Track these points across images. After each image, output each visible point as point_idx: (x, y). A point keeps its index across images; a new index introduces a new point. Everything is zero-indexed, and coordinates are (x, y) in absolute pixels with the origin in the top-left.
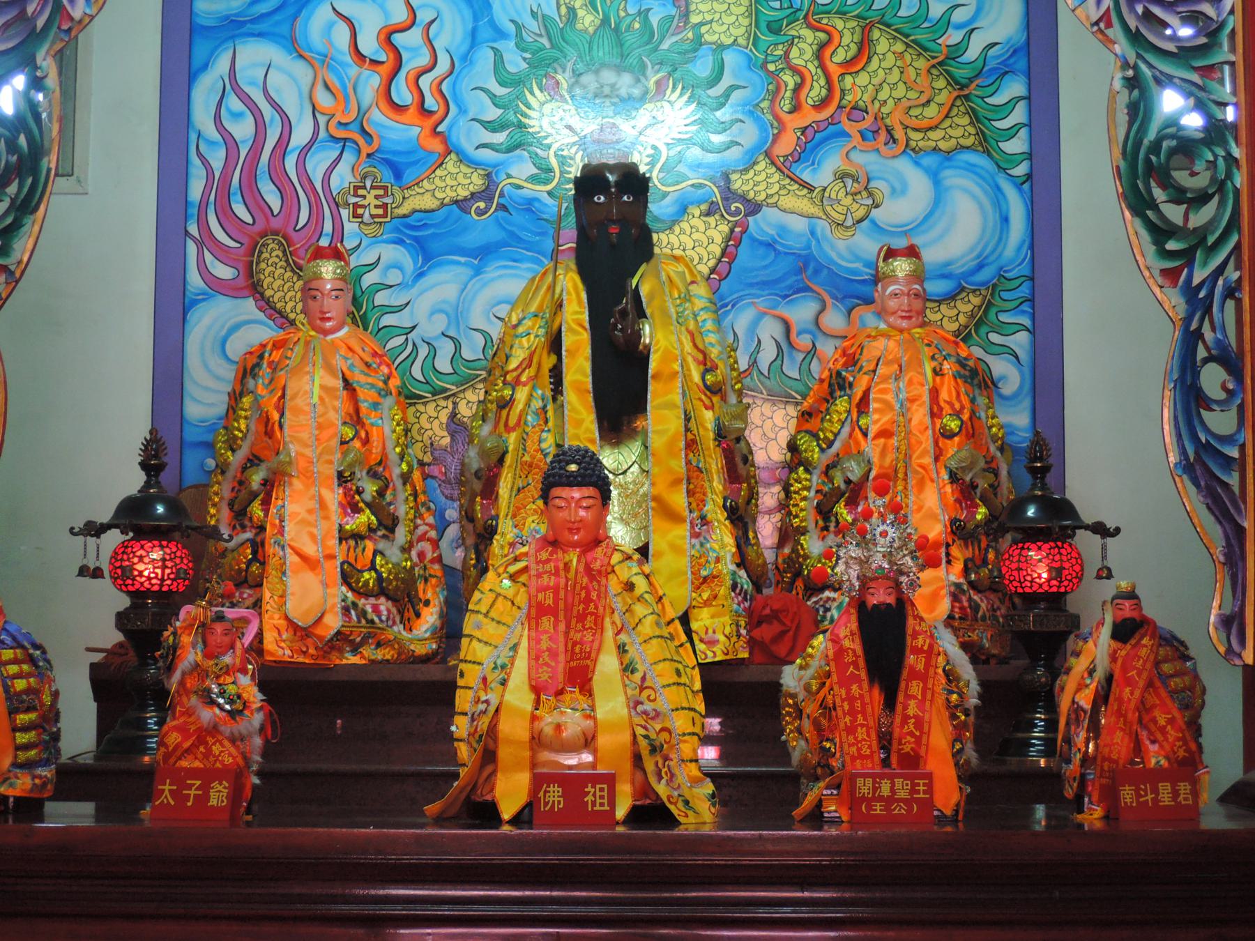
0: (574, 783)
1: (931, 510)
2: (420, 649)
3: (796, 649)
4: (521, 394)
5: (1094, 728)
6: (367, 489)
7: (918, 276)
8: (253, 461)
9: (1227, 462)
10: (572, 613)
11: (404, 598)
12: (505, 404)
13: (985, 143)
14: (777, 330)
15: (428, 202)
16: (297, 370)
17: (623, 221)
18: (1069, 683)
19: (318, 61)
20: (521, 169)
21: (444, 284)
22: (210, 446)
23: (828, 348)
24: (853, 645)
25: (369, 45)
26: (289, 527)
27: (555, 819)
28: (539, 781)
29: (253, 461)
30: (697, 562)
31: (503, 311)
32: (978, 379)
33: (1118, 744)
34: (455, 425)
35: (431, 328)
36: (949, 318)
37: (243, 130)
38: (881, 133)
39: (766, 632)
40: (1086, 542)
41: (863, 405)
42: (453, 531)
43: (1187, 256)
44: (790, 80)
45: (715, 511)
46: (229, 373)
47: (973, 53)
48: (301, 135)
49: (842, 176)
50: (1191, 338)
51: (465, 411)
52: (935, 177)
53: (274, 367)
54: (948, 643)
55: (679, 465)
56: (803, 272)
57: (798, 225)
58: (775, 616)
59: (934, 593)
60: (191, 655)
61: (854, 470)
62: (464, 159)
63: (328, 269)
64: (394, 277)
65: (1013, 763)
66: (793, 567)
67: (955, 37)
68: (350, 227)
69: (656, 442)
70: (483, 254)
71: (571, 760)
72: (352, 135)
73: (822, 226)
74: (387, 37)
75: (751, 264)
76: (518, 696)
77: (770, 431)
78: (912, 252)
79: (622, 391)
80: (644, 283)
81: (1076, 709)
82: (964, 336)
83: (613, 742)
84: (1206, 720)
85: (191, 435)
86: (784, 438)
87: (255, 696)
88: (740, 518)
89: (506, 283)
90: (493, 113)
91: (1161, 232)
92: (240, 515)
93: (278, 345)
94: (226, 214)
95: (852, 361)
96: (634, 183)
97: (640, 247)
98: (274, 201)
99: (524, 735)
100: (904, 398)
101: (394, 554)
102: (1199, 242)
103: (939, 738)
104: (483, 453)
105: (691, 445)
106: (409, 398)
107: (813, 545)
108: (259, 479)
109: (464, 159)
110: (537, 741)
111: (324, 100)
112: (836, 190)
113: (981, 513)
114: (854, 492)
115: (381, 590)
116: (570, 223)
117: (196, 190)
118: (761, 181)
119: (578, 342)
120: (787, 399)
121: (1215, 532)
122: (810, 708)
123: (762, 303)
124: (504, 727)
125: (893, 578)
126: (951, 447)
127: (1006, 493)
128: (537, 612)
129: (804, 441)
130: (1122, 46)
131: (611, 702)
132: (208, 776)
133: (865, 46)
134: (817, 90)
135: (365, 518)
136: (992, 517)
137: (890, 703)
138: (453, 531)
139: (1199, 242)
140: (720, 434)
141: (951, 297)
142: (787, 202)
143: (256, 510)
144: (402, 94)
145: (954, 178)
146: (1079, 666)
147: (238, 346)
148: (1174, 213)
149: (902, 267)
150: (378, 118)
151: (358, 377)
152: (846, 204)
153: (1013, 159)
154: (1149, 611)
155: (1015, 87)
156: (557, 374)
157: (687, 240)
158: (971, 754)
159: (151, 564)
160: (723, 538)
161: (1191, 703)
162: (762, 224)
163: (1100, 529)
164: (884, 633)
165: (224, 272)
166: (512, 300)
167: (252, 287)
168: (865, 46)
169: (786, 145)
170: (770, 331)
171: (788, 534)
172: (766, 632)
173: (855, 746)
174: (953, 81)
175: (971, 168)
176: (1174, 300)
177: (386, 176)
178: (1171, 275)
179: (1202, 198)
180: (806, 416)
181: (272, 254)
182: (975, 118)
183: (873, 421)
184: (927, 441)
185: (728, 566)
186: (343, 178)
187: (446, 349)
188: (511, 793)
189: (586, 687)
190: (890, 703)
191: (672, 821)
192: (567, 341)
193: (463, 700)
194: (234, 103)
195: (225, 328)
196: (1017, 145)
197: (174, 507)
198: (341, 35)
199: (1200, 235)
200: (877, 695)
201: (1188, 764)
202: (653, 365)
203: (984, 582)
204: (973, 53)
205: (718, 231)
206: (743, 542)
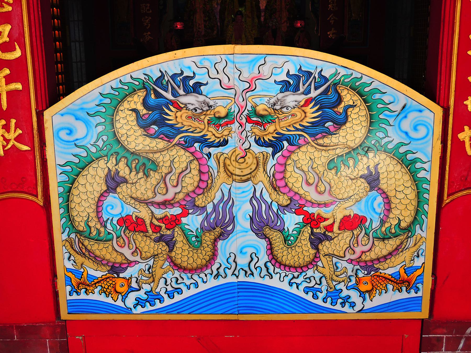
135: (207, 19)
160: (256, 20)
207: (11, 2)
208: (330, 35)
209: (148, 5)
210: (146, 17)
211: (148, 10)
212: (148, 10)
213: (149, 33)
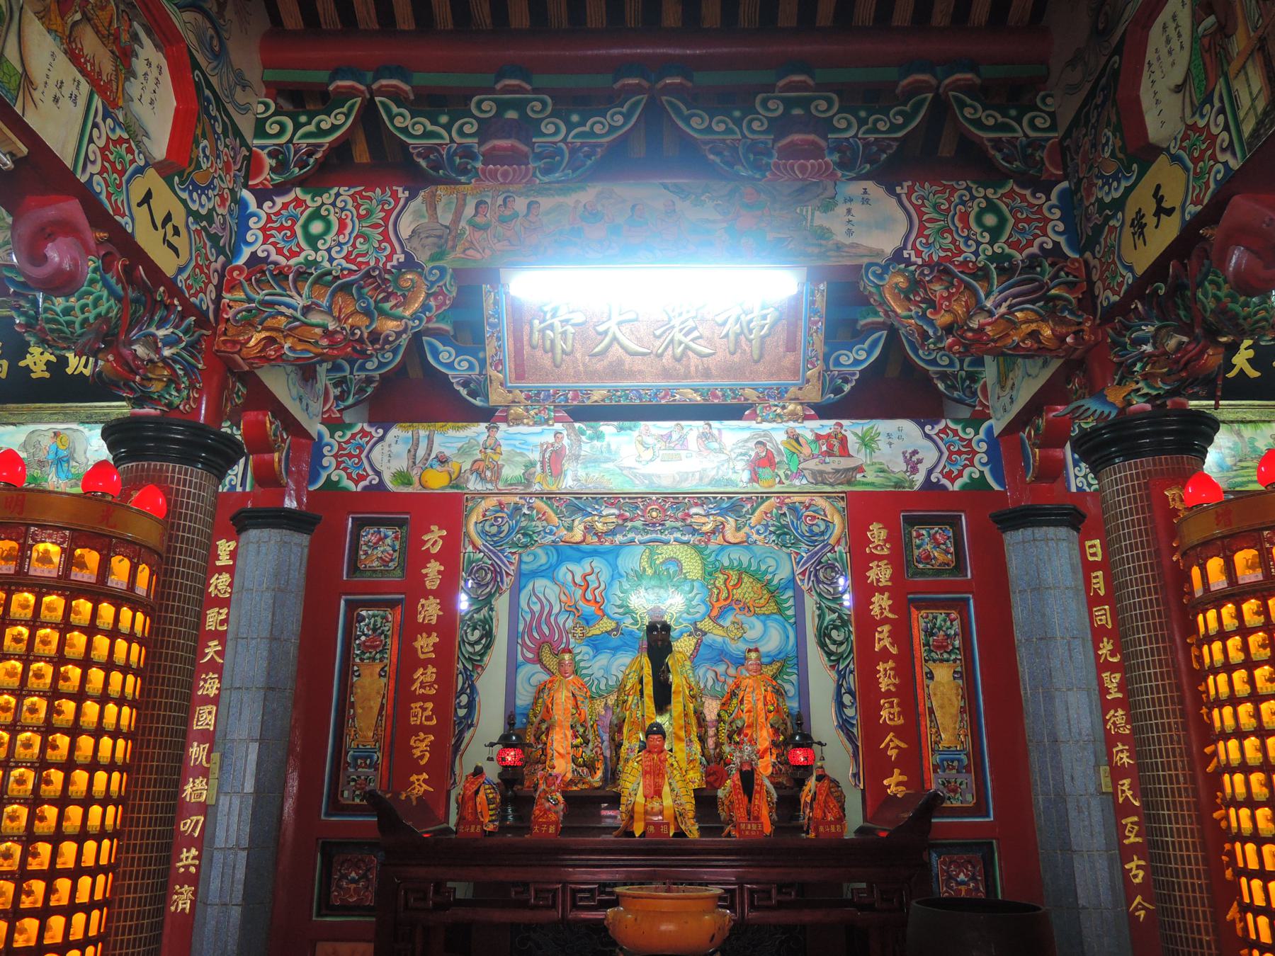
0: (657, 825)
1: (764, 737)
2: (596, 785)
3: (722, 784)
4: (630, 698)
5: (811, 808)
6: (580, 729)
7: (758, 658)
8: (543, 721)
9: (853, 725)
10: (655, 774)
11: (591, 767)
12: (625, 702)
13: (780, 611)
14: (713, 675)
15: (598, 632)
16: (557, 691)
17: (663, 640)
18: (804, 794)
19: (562, 585)
20: (628, 621)
21: (603, 659)
22: (527, 716)
23: (730, 681)
24: (739, 783)
25: (578, 580)
26: (555, 744)
27: (652, 835)
28: (647, 825)
29: (543, 721)
30: (689, 755)
31: (623, 668)
32: (779, 692)
33: (819, 813)
34: (606, 707)
35: (599, 674)
36: (769, 671)
37: (537, 608)
38: (746, 608)
39: (712, 779)
40: (815, 747)
41: (741, 702)
42: (606, 743)
43: (838, 661)
44: (716, 591)
45: (694, 737)
46: (534, 690)
47: (775, 582)
48: (556, 610)
49: (733, 623)
50: (840, 686)
51: (610, 702)
52: (764, 623)
53: (550, 689)
54: (767, 782)
55: (682, 722)
56: (721, 655)
57: (720, 639)
58: (714, 773)
59: (765, 767)
60: (543, 787)
61: (740, 724)
62: (609, 617)
63: (567, 657)
64: (586, 657)
65: (794, 823)
66: (720, 757)
67: (769, 577)
68: (572, 640)
69: (675, 714)
70: (615, 650)
71: (656, 819)
72: (573, 610)
73: (727, 639)
74: (584, 577)
75: (705, 653)
76: (640, 799)
77: (711, 709)
78: (756, 650)
79: (663, 698)
80: (670, 660)
81: (806, 802)
82: (775, 677)
83: (668, 813)
84: (846, 806)
85: (518, 711)
86: (716, 712)
87: (561, 799)
88: (702, 740)
89: (624, 659)
90: (619, 603)
91: (829, 654)
92: (538, 739)
93: (551, 682)
94: (531, 637)
95: (738, 687)
96: (666, 628)
97: (668, 649)
98: (547, 632)
99: (642, 811)
100: (755, 698)
101: (588, 752)
102: (841, 657)
103: (765, 812)
104: (618, 718)
105: (686, 715)
106: (592, 698)
107: (726, 749)
108: (545, 727)
109: (609, 617)
110: (646, 813)
111: (563, 598)
112: (732, 628)
113: (782, 738)
114: (740, 731)
115: (585, 765)
116: (645, 642)
117: (521, 628)
118: (706, 625)
119: (648, 679)
120: (716, 698)
121: (849, 746)
122: (726, 802)
123: (708, 665)
124: (637, 808)
125: (750, 762)
126: (771, 716)
127: (790, 731)
128: (645, 773)
129: (723, 713)
130: (816, 597)
131: (668, 801)
132: (549, 824)
133: (740, 580)
134: (724, 595)
135: (579, 740)
136: (785, 739)
137: (750, 801)
138: (606, 743)
139: (841, 657)
140: (695, 712)
141: (771, 663)
142: (715, 632)
143: (544, 737)
144: (589, 596)
145: (769, 623)
146: (806, 789)
147: (534, 681)
148: (833, 648)
149: (753, 655)
150: (581, 604)
151: (576, 692)
152: (735, 633)
153: (790, 617)
154: (827, 772)
155: (790, 593)
156: (642, 692)
157: (683, 645)
158: (775, 816)
159: (510, 757)
160: (697, 747)
161: (841, 800)
162: (708, 639)
163: (820, 743)
164: (748, 779)
165: (530, 655)
166: (627, 665)
167: (538, 660)
168: (740, 580)
169: (715, 613)
170: (710, 675)
171: (718, 745)
172: (712, 779)
173: (740, 814)
174: (769, 591)
175: (776, 620)
176: (834, 675)
177: (583, 622)
178: (833, 667)
179: (841, 643)
180: (723, 704)
181: (546, 649)
182: (777, 603)
183: (745, 707)
184: (763, 715)
185: (698, 756)
186: (569, 624)
187: (603, 681)
188: (638, 829)
189: (660, 797)
190: (750, 801)
191: (685, 836)
192: (645, 680)
193: (623, 800)
194: (534, 599)
195: (531, 676)
196: (791, 612)
197: (518, 737)
198: (569, 577)
199: (842, 654)
200: (746, 798)
201: (841, 819)
202: (673, 689)
203: (783, 761)
204: (775, 582)
205: (693, 641)
206: (703, 748)
207: (324, 948)
208: (889, 787)
209: (430, 705)
210: (422, 735)
211: (429, 718)
212: (429, 718)
213: (425, 776)
